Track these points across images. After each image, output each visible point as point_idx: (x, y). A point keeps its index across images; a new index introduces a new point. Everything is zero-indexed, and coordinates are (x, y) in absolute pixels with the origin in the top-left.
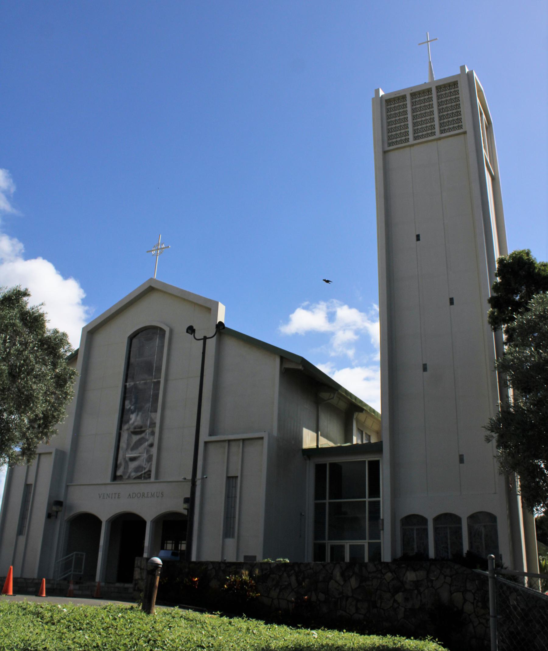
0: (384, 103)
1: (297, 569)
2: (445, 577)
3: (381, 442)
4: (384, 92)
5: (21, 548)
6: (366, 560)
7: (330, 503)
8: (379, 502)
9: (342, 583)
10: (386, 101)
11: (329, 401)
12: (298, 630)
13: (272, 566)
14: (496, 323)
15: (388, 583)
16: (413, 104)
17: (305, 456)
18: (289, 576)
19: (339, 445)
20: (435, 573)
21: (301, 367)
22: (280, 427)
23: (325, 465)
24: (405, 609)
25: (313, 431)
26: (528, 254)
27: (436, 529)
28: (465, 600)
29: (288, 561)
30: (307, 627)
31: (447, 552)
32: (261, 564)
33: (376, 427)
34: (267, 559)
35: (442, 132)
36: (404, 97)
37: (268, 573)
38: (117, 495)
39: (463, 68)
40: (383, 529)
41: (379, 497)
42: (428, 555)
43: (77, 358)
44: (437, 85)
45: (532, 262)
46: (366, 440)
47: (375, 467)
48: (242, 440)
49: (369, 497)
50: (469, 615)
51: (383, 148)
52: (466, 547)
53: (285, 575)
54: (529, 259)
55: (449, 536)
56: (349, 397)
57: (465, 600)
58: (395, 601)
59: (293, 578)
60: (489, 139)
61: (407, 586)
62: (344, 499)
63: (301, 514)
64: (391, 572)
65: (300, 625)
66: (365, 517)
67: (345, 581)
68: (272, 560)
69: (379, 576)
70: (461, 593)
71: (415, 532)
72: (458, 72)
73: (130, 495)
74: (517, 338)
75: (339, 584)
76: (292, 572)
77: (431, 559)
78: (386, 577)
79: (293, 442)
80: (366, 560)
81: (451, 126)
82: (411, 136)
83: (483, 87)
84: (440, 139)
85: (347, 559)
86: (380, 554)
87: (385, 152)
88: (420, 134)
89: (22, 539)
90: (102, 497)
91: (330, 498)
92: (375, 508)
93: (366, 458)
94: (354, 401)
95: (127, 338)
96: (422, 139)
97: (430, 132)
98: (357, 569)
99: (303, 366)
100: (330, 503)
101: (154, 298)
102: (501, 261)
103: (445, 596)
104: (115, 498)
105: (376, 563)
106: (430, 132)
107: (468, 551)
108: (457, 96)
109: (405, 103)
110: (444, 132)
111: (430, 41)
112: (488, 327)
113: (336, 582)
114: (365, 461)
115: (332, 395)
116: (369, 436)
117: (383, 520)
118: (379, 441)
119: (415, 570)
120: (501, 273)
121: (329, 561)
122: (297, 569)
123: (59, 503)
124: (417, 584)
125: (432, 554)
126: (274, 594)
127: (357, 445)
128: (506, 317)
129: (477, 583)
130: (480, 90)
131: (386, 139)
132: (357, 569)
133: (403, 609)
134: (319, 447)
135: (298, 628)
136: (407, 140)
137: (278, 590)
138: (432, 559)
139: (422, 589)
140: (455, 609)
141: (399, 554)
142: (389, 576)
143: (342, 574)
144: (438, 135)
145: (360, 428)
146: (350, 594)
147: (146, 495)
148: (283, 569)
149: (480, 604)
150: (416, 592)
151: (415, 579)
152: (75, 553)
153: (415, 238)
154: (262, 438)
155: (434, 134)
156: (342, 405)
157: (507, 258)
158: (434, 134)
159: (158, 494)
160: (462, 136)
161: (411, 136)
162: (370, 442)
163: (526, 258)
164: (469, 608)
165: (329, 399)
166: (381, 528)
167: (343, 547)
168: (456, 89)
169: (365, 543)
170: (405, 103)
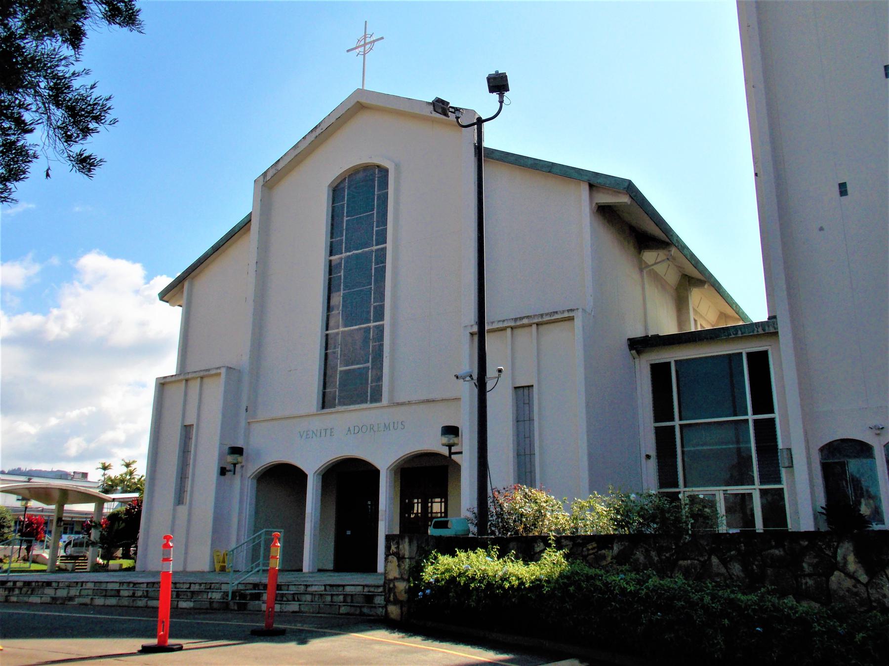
9: (864, 578)
23: (669, 364)
38: (328, 432)
43: (249, 229)
47: (759, 362)
48: (535, 325)
49: (754, 413)
53: (715, 560)
62: (686, 420)
73: (349, 430)
74: (172, 547)
75: (859, 581)
89: (183, 510)
92: (766, 431)
93: (743, 349)
101: (363, 120)
123: (237, 451)
147: (375, 428)
152: (264, 530)
169: (755, 490)
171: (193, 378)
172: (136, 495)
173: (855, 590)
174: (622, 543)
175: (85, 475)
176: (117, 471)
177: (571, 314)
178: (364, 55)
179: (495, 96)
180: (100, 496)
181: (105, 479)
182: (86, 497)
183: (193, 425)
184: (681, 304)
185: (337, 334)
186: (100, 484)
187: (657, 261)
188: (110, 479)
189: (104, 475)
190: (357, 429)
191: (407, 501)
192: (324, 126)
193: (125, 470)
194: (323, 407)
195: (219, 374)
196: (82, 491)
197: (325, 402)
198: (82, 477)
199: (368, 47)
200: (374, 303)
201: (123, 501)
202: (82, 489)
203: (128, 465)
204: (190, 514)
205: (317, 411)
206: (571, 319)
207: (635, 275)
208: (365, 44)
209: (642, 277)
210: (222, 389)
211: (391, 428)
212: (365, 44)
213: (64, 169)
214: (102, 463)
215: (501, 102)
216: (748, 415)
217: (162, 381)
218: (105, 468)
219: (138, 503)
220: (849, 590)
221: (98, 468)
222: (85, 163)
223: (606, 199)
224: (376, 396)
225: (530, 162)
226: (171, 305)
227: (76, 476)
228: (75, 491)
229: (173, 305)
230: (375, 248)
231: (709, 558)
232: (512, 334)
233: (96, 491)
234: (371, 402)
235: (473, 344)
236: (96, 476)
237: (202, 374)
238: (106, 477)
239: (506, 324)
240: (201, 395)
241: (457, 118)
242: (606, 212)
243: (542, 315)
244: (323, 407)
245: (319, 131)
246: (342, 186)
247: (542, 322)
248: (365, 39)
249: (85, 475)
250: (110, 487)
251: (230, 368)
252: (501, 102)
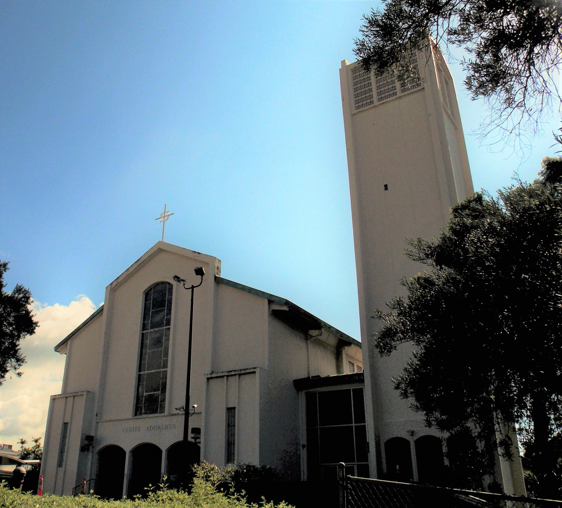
5: (61, 474)
8: (365, 426)
21: (285, 308)
41: (365, 423)
43: (102, 314)
47: (359, 394)
87: (353, 115)
89: (62, 469)
90: (125, 431)
92: (362, 431)
95: (142, 294)
96: (370, 105)
97: (392, 92)
104: (136, 431)
106: (392, 92)
114: (350, 389)
156: (333, 341)
158: (395, 94)
159: (171, 426)
160: (421, 93)
171: (70, 397)
172: (38, 461)
175: (10, 447)
176: (30, 445)
177: (254, 370)
178: (164, 222)
179: (200, 276)
180: (19, 461)
181: (22, 450)
182: (11, 462)
183: (68, 423)
184: (338, 356)
185: (145, 374)
186: (19, 453)
188: (25, 449)
189: (22, 447)
190: (152, 428)
191: (560, 439)
192: (142, 260)
193: (34, 444)
194: (136, 415)
195: (83, 395)
196: (10, 458)
197: (138, 411)
198: (9, 448)
199: (166, 218)
200: (163, 358)
201: (32, 464)
202: (10, 456)
203: (36, 441)
204: (65, 471)
205: (132, 417)
206: (254, 372)
207: (302, 344)
208: (164, 217)
209: (307, 344)
210: (84, 403)
211: (169, 427)
212: (164, 217)
213: (15, 376)
214: (21, 440)
215: (202, 279)
217: (54, 398)
218: (23, 443)
219: (39, 464)
221: (18, 443)
222: (19, 374)
223: (276, 307)
224: (162, 411)
225: (241, 286)
226: (60, 354)
227: (5, 447)
228: (6, 458)
229: (62, 354)
230: (165, 327)
232: (227, 379)
233: (17, 458)
234: (160, 413)
235: (208, 383)
236: (17, 448)
237: (74, 394)
238: (23, 448)
239: (224, 374)
241: (184, 284)
242: (276, 314)
243: (241, 370)
244: (136, 415)
245: (139, 262)
246: (150, 292)
247: (242, 374)
248: (165, 213)
249: (10, 447)
250: (25, 456)
251: (89, 392)
252: (202, 279)
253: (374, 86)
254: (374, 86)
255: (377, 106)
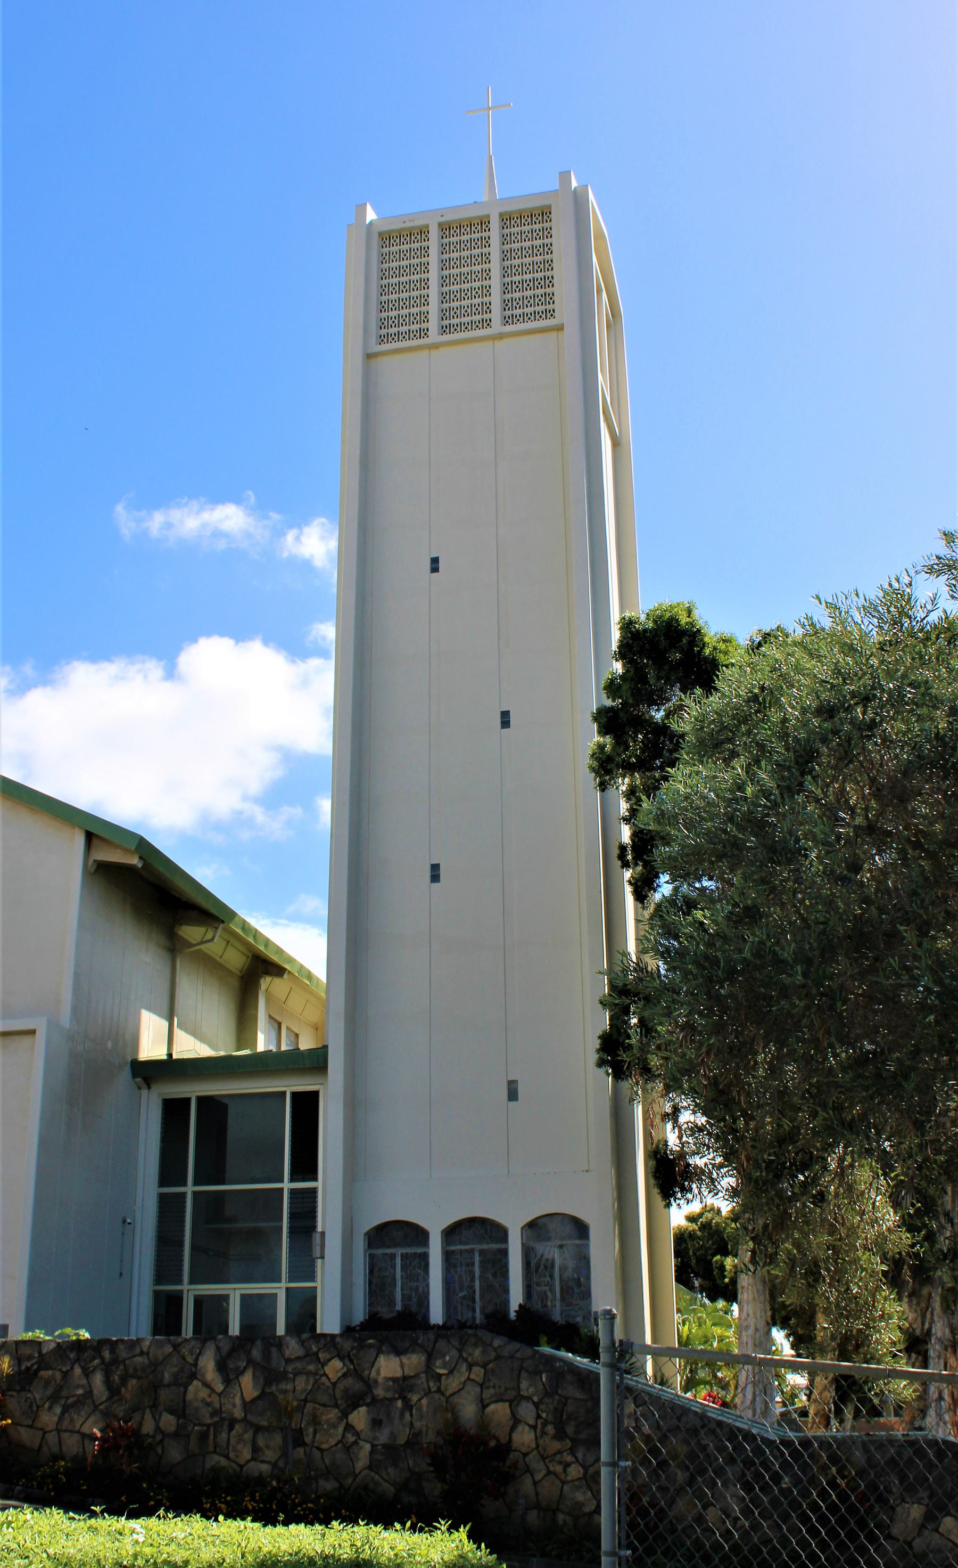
0: (375, 240)
1: (107, 1354)
2: (470, 1368)
3: (325, 1047)
4: (377, 214)
6: (281, 1330)
7: (195, 1194)
8: (314, 1191)
9: (219, 1387)
10: (380, 234)
11: (202, 947)
12: (93, 1520)
13: (45, 1350)
14: (608, 772)
15: (334, 1384)
16: (443, 249)
17: (139, 1080)
18: (87, 1373)
19: (222, 1053)
20: (447, 1358)
21: (135, 861)
22: (75, 1009)
23: (187, 1101)
24: (373, 1446)
25: (160, 1016)
26: (689, 612)
27: (448, 1256)
28: (516, 1421)
29: (87, 1335)
30: (115, 1511)
31: (474, 1310)
32: (17, 1343)
33: (312, 1014)
34: (33, 1331)
35: (506, 321)
36: (423, 231)
37: (35, 1367)
39: (565, 177)
40: (323, 1257)
41: (316, 1179)
42: (426, 1317)
44: (503, 210)
45: (699, 631)
46: (287, 1045)
49: (292, 1180)
50: (525, 1455)
51: (365, 345)
52: (516, 1297)
53: (78, 1370)
54: (692, 624)
55: (477, 1273)
56: (251, 940)
57: (516, 1421)
58: (349, 1427)
59: (98, 1379)
60: (613, 348)
61: (380, 1392)
62: (231, 1184)
63: (124, 1221)
64: (342, 1359)
65: (98, 1509)
66: (281, 1228)
67: (227, 1382)
68: (46, 1334)
69: (311, 1367)
70: (507, 1404)
71: (398, 1261)
72: (555, 185)
75: (213, 1390)
76: (96, 1362)
77: (434, 1325)
78: (327, 1369)
79: (110, 1045)
80: (281, 1330)
81: (528, 310)
82: (433, 324)
83: (607, 230)
84: (501, 336)
85: (235, 1329)
86: (314, 1316)
87: (369, 356)
88: (455, 321)
91: (196, 1183)
93: (287, 1086)
94: (262, 948)
98: (256, 1353)
99: (141, 858)
100: (195, 1194)
102: (627, 626)
103: (468, 1410)
105: (305, 1336)
107: (520, 1306)
108: (546, 241)
109: (424, 244)
110: (510, 321)
111: (493, 107)
112: (591, 780)
113: (206, 1385)
114: (284, 1093)
115: (209, 936)
116: (297, 1035)
117: (323, 1233)
118: (320, 1046)
119: (398, 1352)
120: (624, 652)
121: (190, 1334)
122: (107, 1354)
124: (403, 1385)
125: (436, 1314)
126: (48, 1419)
127: (267, 1053)
128: (630, 757)
129: (544, 1379)
130: (600, 236)
131: (373, 326)
132: (256, 1353)
133: (368, 1447)
134: (174, 1057)
135: (93, 1515)
136: (423, 333)
137: (58, 1410)
138: (437, 1327)
139: (414, 1398)
140: (493, 1444)
141: (359, 1315)
142: (335, 1367)
143: (221, 1367)
144: (497, 326)
145: (274, 1016)
146: (238, 1413)
148: (72, 1356)
149: (550, 1429)
150: (399, 1403)
151: (399, 1374)
153: (427, 565)
154: (32, 1032)
155: (488, 323)
156: (235, 960)
157: (643, 618)
158: (488, 323)
160: (553, 335)
161: (433, 324)
162: (299, 1049)
163: (684, 620)
164: (524, 1437)
165: (202, 942)
166: (318, 1255)
167: (226, 1298)
168: (546, 225)
169: (279, 1289)
170: (424, 244)
173: (209, 1400)
174: (886, 1381)
187: (206, 939)
216: (283, 1182)
220: (203, 1400)
231: (72, 1368)
240: (615, 344)
253: (495, 250)
254: (495, 250)
255: (435, 346)
